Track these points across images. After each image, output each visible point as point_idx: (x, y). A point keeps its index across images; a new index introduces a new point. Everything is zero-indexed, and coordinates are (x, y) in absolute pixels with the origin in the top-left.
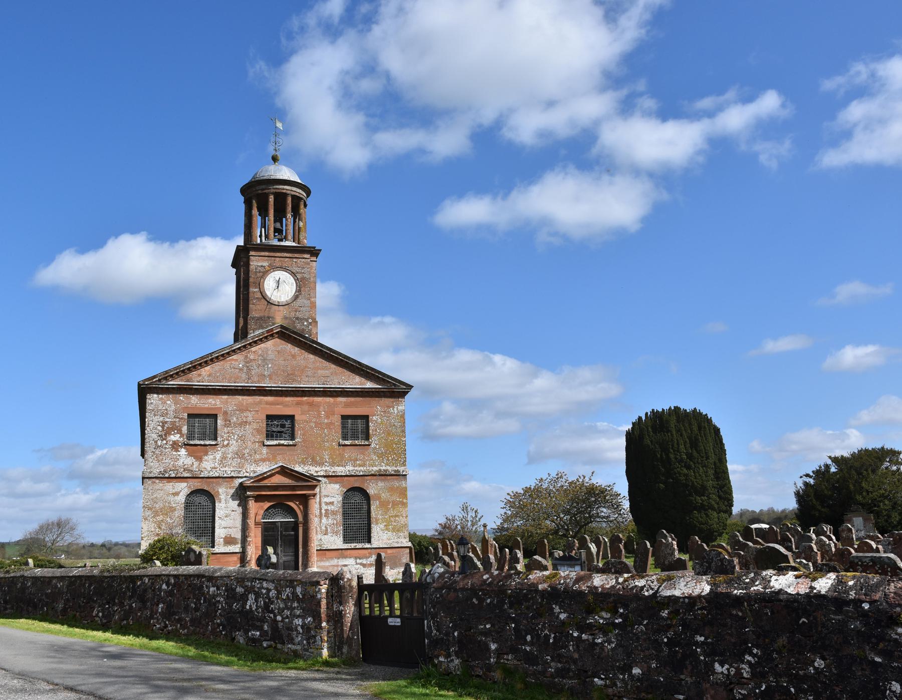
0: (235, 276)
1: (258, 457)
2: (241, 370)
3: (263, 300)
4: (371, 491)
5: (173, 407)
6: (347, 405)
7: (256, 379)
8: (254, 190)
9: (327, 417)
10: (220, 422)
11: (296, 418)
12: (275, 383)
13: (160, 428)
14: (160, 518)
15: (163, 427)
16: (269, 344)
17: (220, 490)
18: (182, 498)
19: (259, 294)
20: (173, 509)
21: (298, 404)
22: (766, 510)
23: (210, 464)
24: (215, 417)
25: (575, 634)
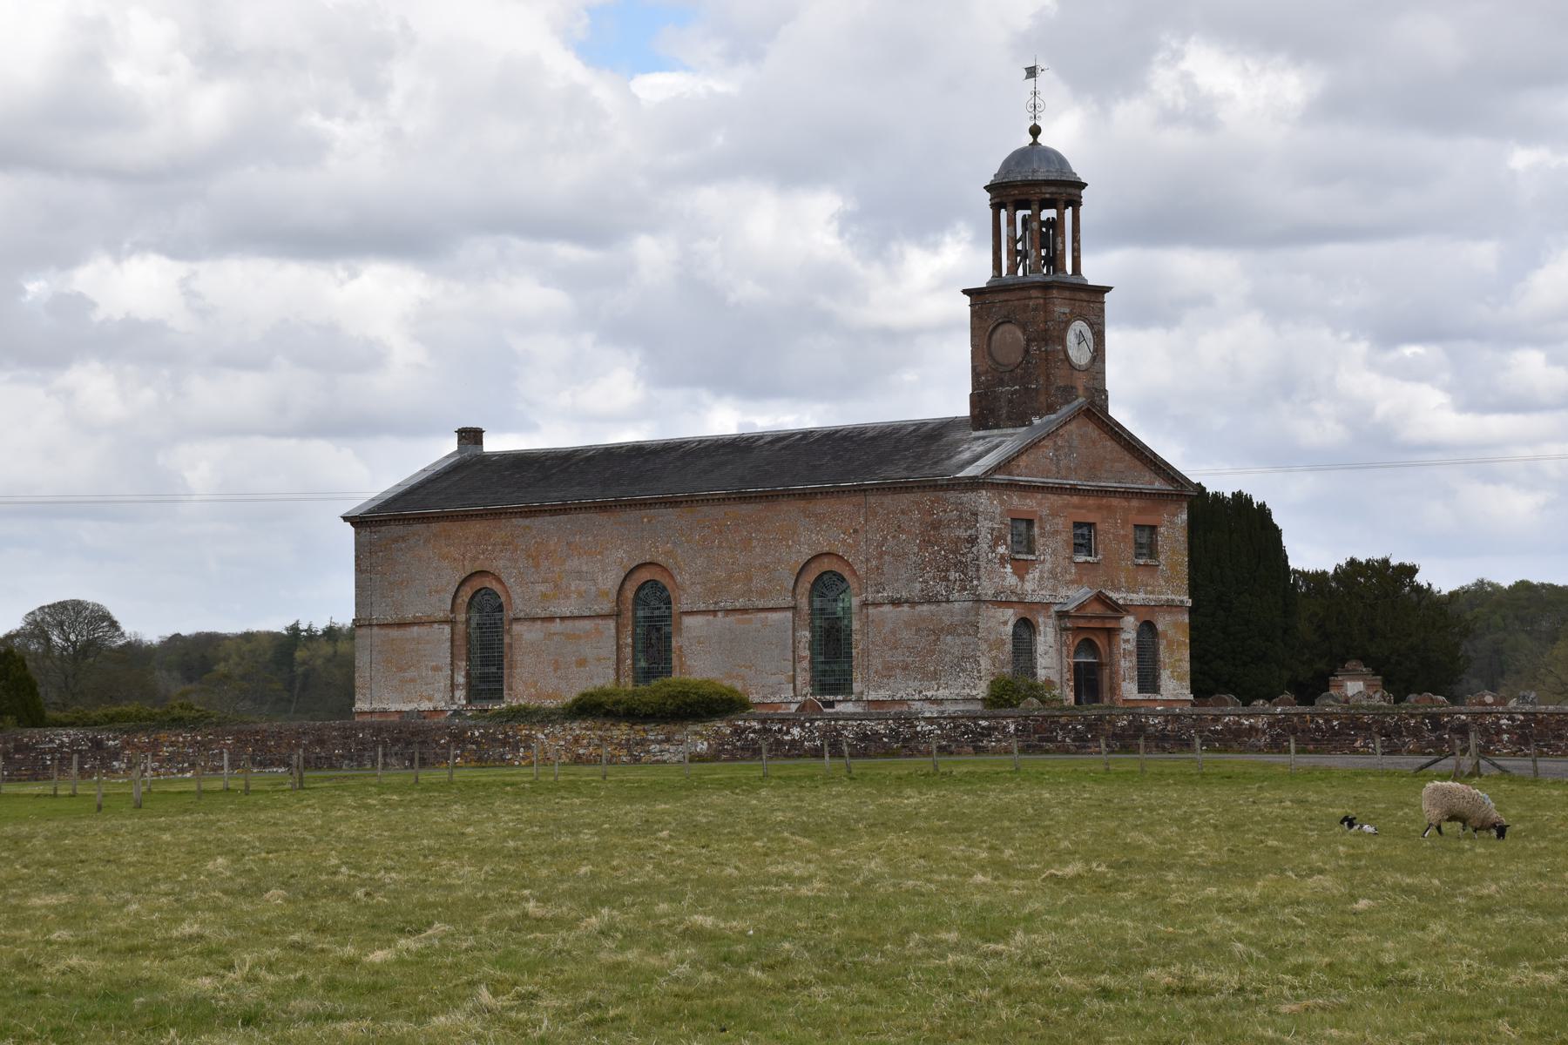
0: (1195, 480)
1: (1068, 577)
2: (1052, 460)
3: (1066, 363)
4: (1160, 627)
5: (999, 510)
6: (1140, 511)
7: (1063, 473)
8: (1038, 190)
9: (1123, 528)
10: (1036, 530)
11: (1099, 527)
12: (1080, 480)
13: (989, 536)
14: (994, 653)
15: (992, 535)
16: (1072, 427)
17: (1041, 620)
18: (1009, 629)
19: (1062, 353)
20: (1003, 643)
21: (1099, 508)
22: (1445, 592)
23: (1032, 586)
24: (1030, 523)
25: (953, 877)
